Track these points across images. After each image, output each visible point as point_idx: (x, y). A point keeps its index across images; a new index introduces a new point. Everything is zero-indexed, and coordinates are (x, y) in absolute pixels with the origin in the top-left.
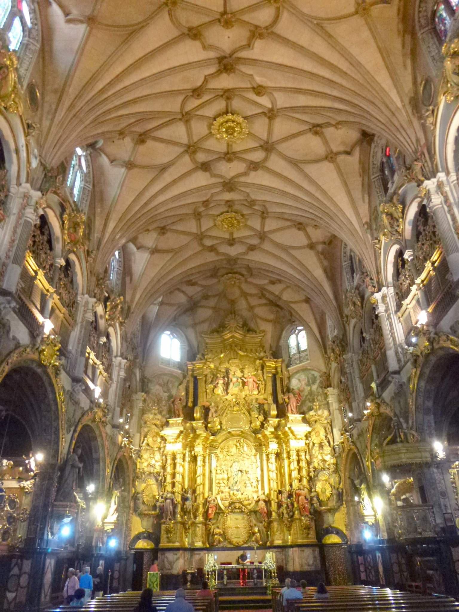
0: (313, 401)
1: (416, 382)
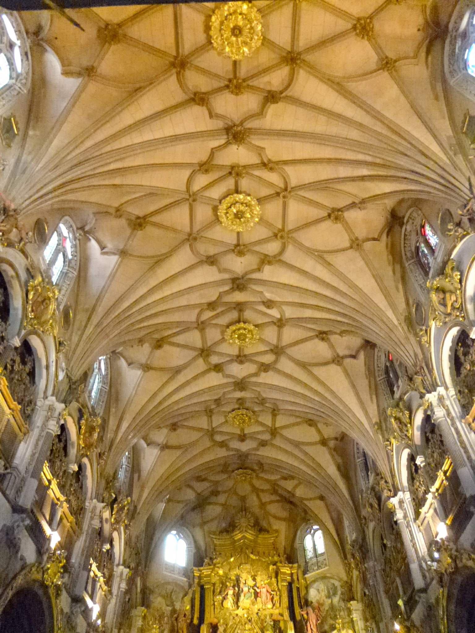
0: (335, 618)
1: (445, 604)
